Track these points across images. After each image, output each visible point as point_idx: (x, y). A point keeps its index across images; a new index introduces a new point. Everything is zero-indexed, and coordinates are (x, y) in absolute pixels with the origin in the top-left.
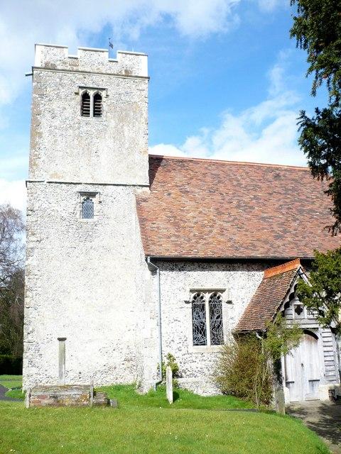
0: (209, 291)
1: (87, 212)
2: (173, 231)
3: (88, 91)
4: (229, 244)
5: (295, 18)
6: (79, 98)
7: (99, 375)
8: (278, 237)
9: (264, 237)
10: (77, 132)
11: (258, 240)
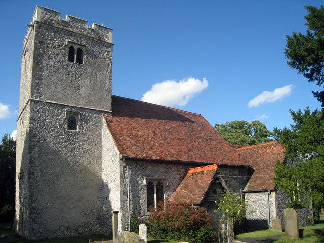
0: (157, 179)
1: (72, 124)
2: (133, 142)
3: (82, 47)
4: (167, 153)
5: (285, 49)
6: (67, 50)
7: (80, 228)
8: (190, 151)
9: (183, 150)
10: (65, 71)
11: (181, 151)
